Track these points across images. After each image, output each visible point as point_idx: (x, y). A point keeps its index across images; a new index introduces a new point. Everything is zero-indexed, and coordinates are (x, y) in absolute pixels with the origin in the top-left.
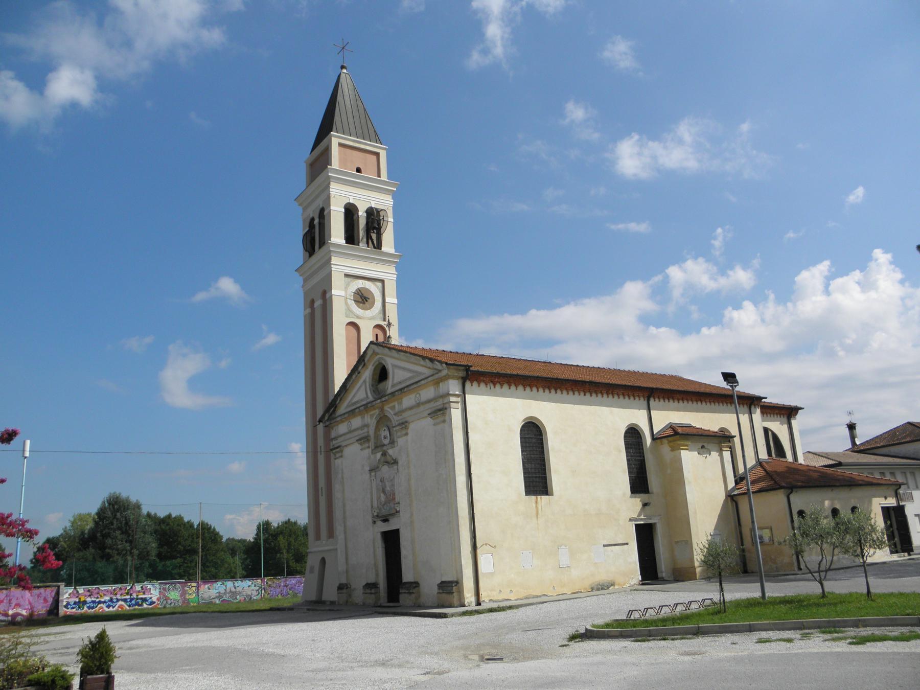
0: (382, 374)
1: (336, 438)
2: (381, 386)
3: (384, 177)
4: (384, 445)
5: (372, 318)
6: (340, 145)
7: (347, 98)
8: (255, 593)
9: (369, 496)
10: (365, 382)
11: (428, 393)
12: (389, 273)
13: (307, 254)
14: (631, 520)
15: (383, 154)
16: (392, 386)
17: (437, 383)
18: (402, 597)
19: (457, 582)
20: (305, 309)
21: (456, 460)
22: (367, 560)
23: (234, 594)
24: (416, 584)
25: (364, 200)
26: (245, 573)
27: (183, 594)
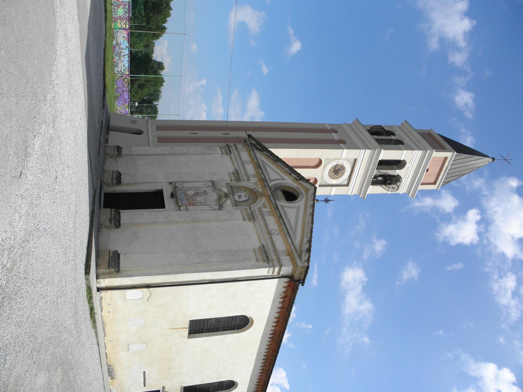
0: (290, 196)
1: (237, 149)
2: (280, 194)
3: (421, 187)
4: (233, 195)
5: (322, 177)
6: (446, 158)
7: (474, 162)
8: (119, 69)
9: (192, 179)
10: (283, 179)
11: (280, 244)
12: (353, 190)
13: (369, 129)
14: (164, 388)
15: (434, 187)
16: (282, 206)
17: (289, 254)
18: (108, 210)
19: (118, 271)
20: (329, 125)
21: (225, 272)
22: (141, 176)
23: (119, 54)
24: (118, 224)
25: (405, 174)
26: (133, 52)
27: (121, 18)
